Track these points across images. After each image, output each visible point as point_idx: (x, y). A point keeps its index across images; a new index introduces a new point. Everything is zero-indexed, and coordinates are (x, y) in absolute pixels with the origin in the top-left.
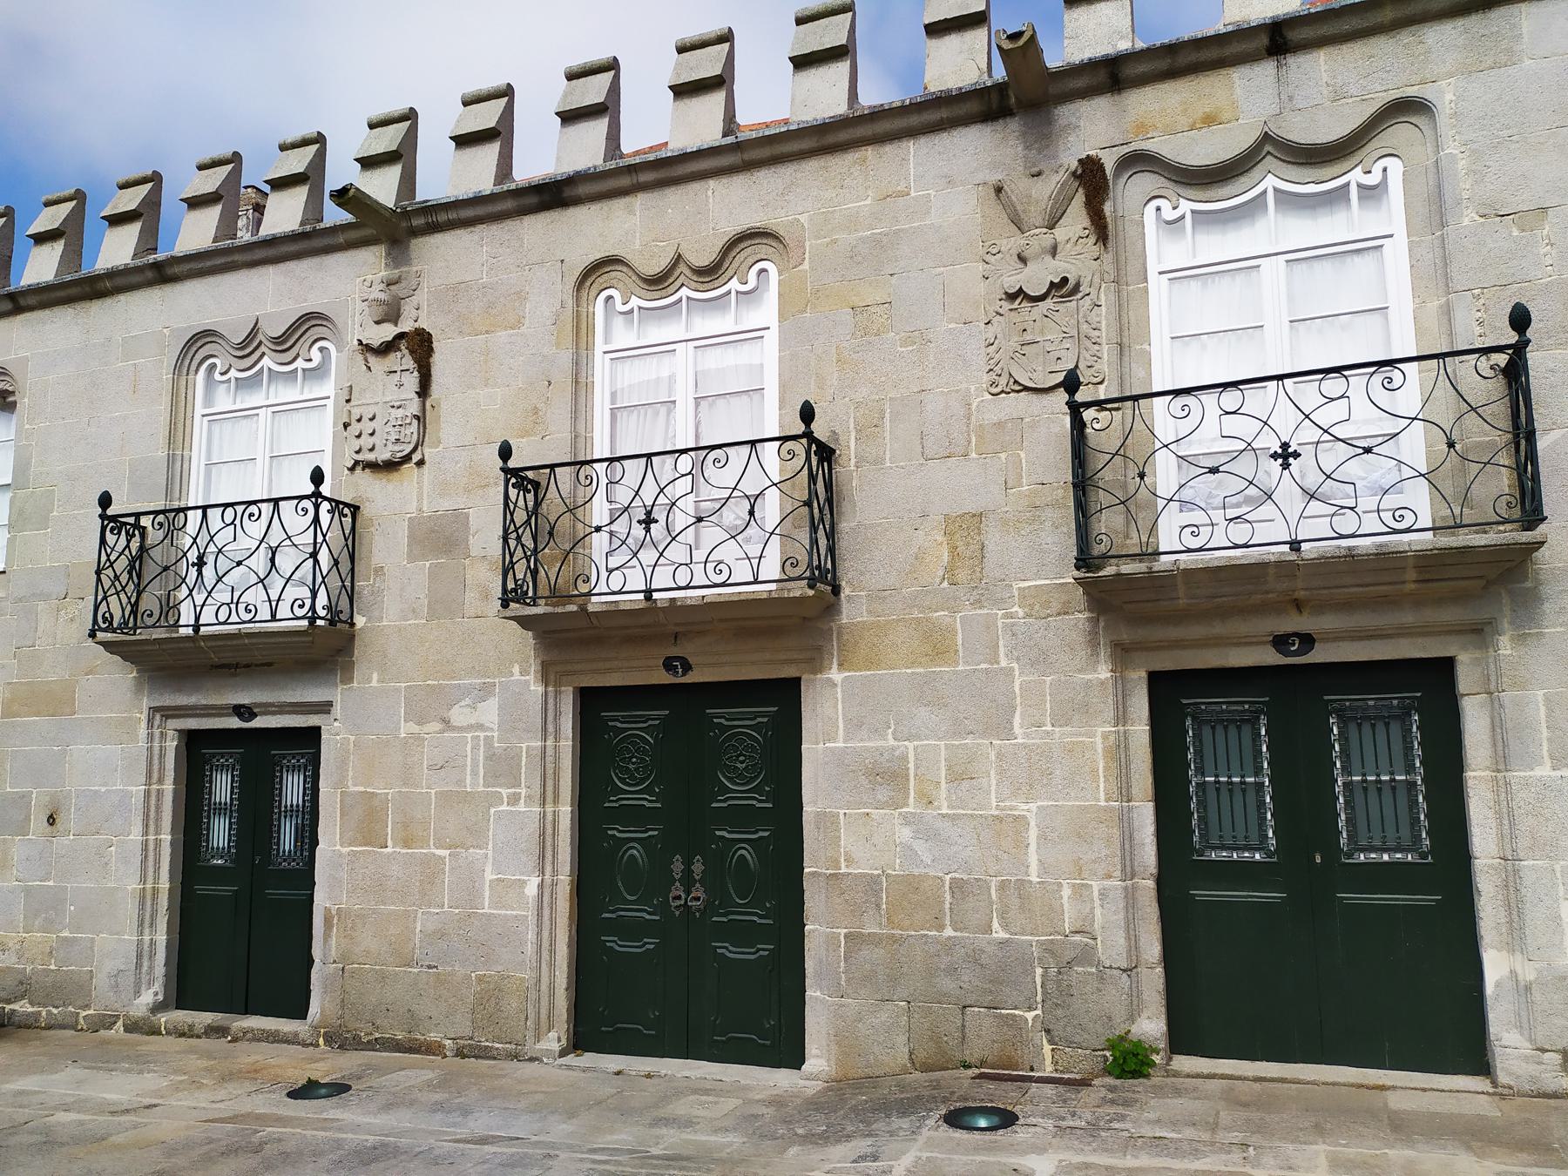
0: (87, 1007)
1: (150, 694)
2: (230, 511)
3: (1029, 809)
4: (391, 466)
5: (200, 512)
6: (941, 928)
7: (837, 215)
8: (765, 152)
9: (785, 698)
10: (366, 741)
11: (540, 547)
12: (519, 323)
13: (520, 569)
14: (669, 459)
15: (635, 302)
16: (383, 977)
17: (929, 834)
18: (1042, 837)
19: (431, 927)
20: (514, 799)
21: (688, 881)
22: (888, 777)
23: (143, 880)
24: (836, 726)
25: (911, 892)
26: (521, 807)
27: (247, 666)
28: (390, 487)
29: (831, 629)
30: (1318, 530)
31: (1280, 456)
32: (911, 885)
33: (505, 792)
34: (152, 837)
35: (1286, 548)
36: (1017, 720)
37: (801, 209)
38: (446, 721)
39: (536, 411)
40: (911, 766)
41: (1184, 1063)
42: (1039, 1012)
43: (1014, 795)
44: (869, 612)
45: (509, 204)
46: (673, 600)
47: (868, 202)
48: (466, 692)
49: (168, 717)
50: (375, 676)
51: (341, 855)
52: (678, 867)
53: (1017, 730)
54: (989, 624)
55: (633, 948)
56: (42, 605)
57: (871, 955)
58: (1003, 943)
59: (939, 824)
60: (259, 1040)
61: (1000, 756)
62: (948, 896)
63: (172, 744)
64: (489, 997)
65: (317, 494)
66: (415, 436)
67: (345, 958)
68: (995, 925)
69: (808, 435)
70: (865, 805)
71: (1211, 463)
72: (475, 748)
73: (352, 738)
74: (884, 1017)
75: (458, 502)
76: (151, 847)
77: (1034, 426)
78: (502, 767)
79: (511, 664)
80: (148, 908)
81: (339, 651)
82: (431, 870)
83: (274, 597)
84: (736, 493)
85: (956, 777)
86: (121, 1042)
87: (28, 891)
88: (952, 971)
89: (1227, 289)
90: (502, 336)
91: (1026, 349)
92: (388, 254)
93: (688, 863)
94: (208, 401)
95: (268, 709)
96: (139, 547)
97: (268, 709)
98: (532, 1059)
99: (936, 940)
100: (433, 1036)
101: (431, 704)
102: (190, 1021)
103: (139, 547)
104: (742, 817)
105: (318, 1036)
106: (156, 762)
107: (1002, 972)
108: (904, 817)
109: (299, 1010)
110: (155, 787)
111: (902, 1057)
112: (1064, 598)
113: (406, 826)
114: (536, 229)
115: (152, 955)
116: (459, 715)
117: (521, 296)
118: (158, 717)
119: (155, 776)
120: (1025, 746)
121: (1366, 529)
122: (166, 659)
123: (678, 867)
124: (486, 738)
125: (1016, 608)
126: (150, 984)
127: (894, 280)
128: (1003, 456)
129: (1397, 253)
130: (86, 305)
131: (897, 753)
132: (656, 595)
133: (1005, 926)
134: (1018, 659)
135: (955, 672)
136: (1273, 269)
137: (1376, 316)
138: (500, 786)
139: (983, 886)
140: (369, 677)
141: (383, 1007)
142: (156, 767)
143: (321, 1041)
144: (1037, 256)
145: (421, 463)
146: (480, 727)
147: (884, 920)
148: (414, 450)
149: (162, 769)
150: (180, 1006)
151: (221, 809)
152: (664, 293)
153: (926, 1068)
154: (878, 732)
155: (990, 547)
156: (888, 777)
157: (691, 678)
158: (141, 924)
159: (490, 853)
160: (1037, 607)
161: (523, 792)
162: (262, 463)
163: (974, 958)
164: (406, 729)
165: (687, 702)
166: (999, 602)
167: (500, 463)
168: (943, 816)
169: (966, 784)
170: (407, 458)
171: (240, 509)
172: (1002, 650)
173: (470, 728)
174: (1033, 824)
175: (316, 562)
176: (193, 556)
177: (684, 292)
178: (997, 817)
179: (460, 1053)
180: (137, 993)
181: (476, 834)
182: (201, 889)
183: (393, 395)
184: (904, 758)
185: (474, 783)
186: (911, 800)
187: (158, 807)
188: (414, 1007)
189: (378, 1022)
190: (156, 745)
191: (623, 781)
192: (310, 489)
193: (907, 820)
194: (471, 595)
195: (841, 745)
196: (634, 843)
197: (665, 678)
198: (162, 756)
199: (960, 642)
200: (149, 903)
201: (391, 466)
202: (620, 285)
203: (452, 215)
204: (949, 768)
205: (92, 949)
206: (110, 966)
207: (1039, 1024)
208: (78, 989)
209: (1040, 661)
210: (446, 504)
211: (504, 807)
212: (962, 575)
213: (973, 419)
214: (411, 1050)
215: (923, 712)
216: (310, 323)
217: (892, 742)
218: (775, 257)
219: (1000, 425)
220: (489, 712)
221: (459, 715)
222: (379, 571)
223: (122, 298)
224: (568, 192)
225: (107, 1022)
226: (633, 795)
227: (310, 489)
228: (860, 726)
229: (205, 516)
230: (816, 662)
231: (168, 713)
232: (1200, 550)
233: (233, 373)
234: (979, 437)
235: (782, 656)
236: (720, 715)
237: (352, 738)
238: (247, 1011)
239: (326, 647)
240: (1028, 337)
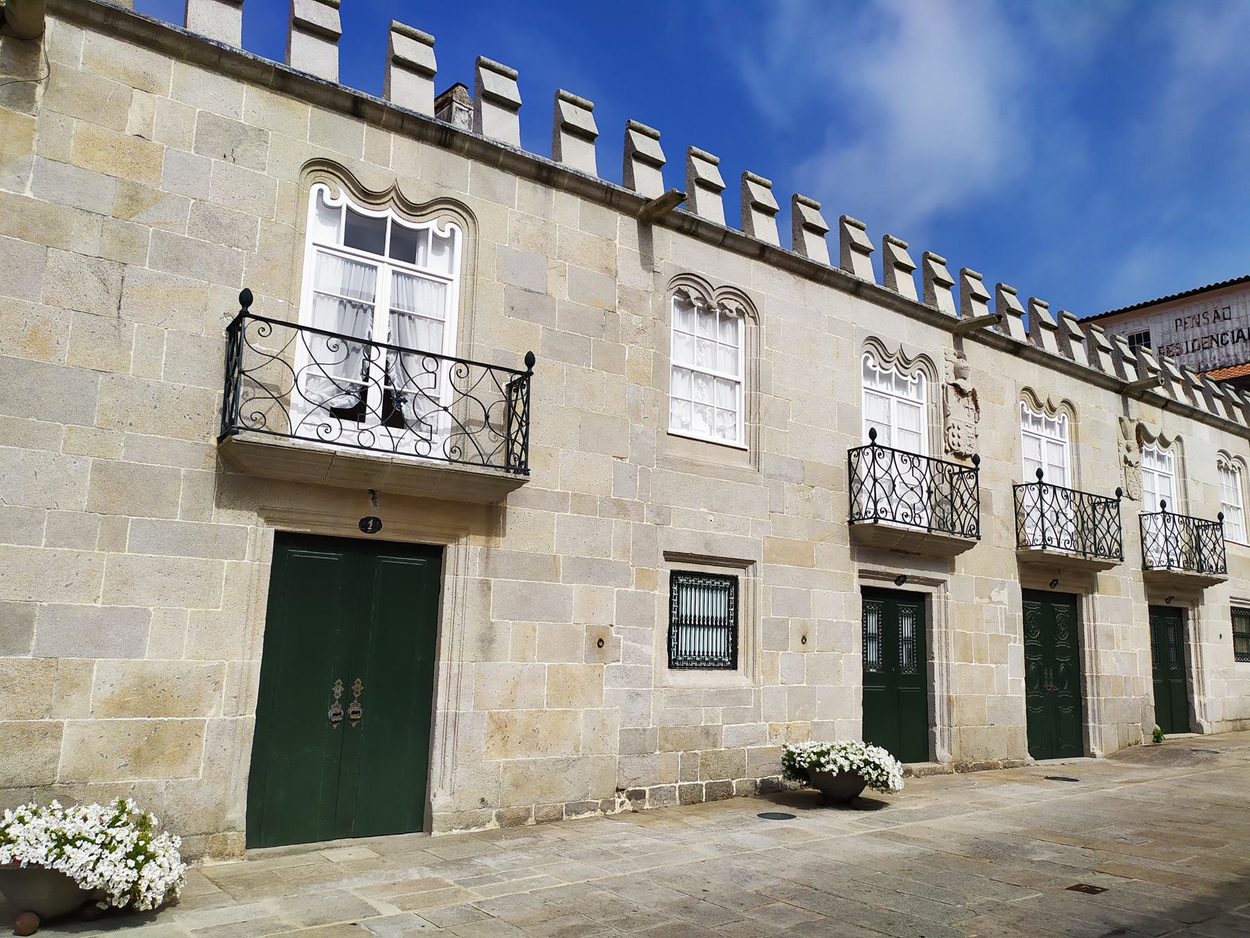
9: (1073, 601)
41: (1166, 736)
45: (599, 194)
56: (786, 485)
65: (873, 444)
87: (791, 690)
100: (995, 760)
116: (995, 596)
146: (1001, 603)
164: (977, 600)
185: (1002, 632)
192: (869, 442)
214: (989, 768)
227: (1037, 480)
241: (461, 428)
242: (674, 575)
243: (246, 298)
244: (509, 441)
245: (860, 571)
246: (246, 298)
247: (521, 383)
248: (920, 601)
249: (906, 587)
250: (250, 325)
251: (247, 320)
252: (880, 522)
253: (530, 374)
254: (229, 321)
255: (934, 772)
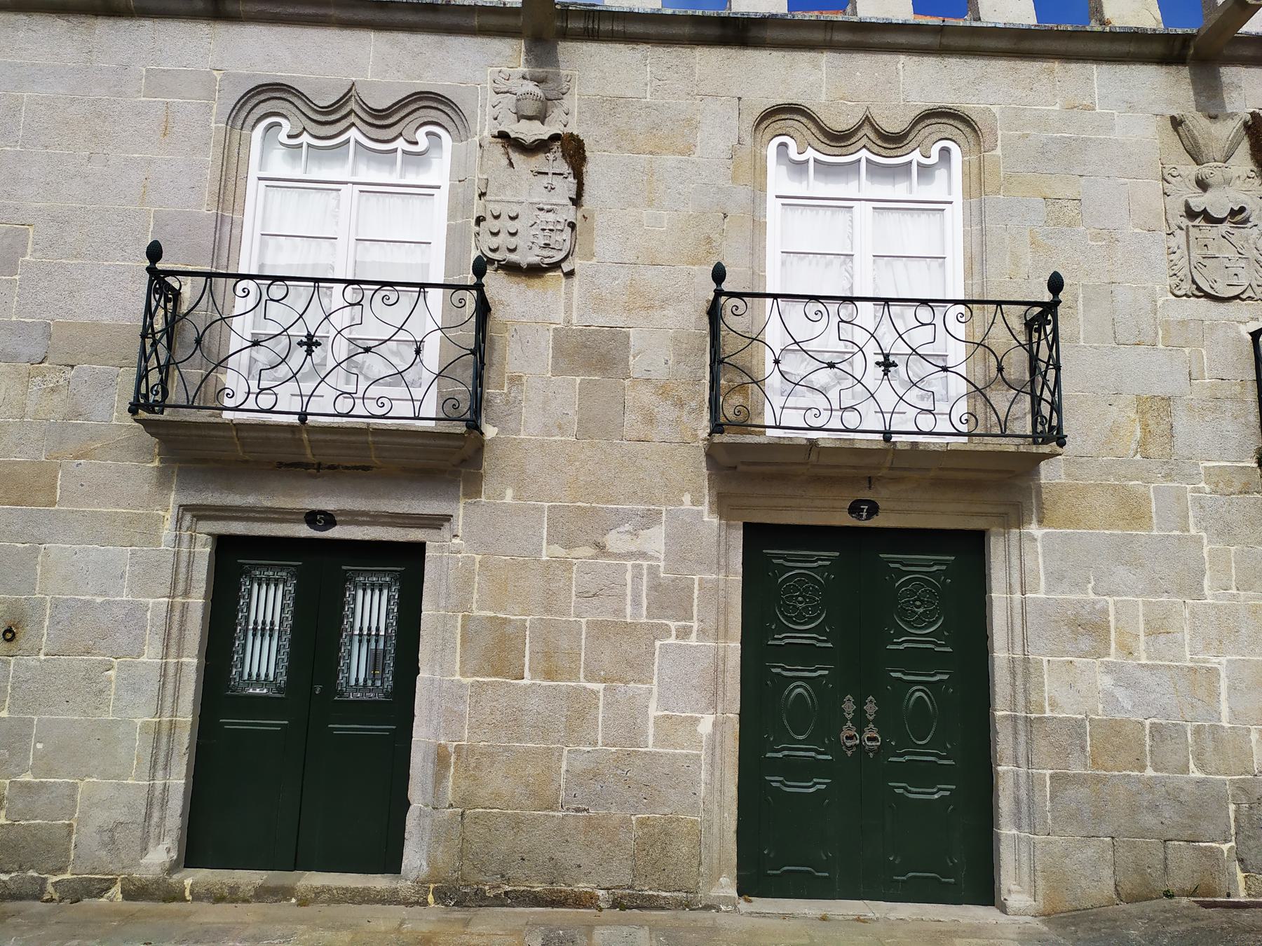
0: (62, 870)
1: (181, 489)
3: (1220, 662)
4: (535, 271)
6: (1142, 768)
7: (1027, 113)
8: (964, 42)
9: (970, 550)
11: (179, 355)
12: (688, 150)
13: (154, 377)
15: (811, 154)
16: (517, 824)
17: (1130, 684)
18: (1232, 688)
19: (579, 766)
20: (684, 633)
21: (860, 721)
22: (1090, 629)
23: (159, 711)
24: (1028, 578)
25: (1114, 738)
26: (693, 641)
27: (332, 467)
28: (530, 293)
29: (1029, 487)
30: (326, 405)
31: (305, 344)
32: (1113, 728)
33: (673, 625)
34: (172, 660)
35: (879, 437)
36: (1206, 583)
37: (992, 100)
38: (600, 547)
39: (709, 240)
40: (1112, 618)
42: (1233, 844)
43: (1207, 647)
44: (1068, 475)
46: (915, 444)
47: (1057, 107)
48: (626, 517)
49: (199, 518)
50: (509, 493)
51: (462, 686)
52: (849, 706)
53: (1206, 591)
54: (1180, 497)
55: (795, 787)
57: (1073, 793)
58: (1199, 783)
59: (1138, 673)
60: (338, 902)
61: (1193, 614)
62: (1147, 739)
63: (204, 551)
64: (655, 842)
66: (568, 243)
67: (466, 801)
68: (1192, 766)
69: (479, 287)
70: (1067, 653)
71: (827, 358)
72: (637, 577)
73: (478, 558)
74: (1090, 852)
75: (618, 320)
76: (171, 671)
77: (1212, 328)
78: (671, 599)
79: (682, 491)
80: (163, 746)
81: (464, 462)
82: (581, 707)
83: (1003, 419)
84: (402, 336)
85: (1154, 631)
86: (118, 913)
88: (1154, 808)
89: (317, 199)
90: (670, 160)
91: (1206, 262)
92: (528, 51)
93: (860, 703)
94: (262, 166)
95: (354, 518)
96: (174, 315)
97: (354, 518)
98: (707, 908)
99: (1139, 780)
100: (582, 886)
101: (583, 526)
102: (231, 882)
103: (174, 315)
104: (920, 660)
105: (427, 892)
106: (183, 570)
107: (1198, 809)
108: (1107, 665)
109: (390, 862)
110: (179, 599)
111: (1109, 890)
112: (1244, 479)
113: (548, 656)
114: (710, 62)
115: (164, 803)
116: (616, 541)
117: (692, 124)
118: (188, 517)
119: (181, 587)
120: (1215, 606)
122: (196, 447)
123: (849, 706)
124: (650, 567)
125: (1202, 485)
126: (159, 839)
127: (1082, 180)
128: (1187, 350)
129: (955, 215)
130: (90, 21)
131: (1097, 607)
132: (895, 438)
133: (1201, 767)
134: (1206, 529)
135: (1150, 537)
136: (863, 211)
137: (935, 263)
138: (668, 618)
139: (1181, 731)
140: (500, 493)
141: (518, 856)
142: (182, 576)
143: (430, 898)
144: (1219, 185)
145: (570, 274)
146: (643, 555)
147: (1089, 762)
148: (566, 257)
149: (189, 579)
150: (188, 865)
151: (263, 631)
152: (844, 150)
153: (1133, 899)
154: (1079, 586)
155: (1178, 428)
156: (1090, 629)
157: (877, 522)
158: (154, 766)
159: (655, 689)
160: (1221, 485)
161: (695, 625)
163: (1174, 796)
165: (861, 546)
166: (1188, 477)
168: (1143, 666)
169: (1162, 638)
170: (556, 266)
172: (1191, 520)
173: (631, 555)
174: (1223, 675)
177: (353, 134)
178: (1191, 669)
179: (617, 904)
180: (144, 850)
181: (638, 667)
182: (231, 723)
183: (542, 198)
184: (1105, 611)
186: (1113, 650)
187: (182, 624)
188: (558, 855)
189: (510, 873)
190: (184, 549)
191: (789, 619)
193: (1109, 669)
194: (629, 418)
195: (1042, 596)
196: (799, 681)
197: (847, 520)
198: (190, 564)
199: (1154, 510)
200: (164, 740)
201: (535, 271)
202: (797, 135)
203: (618, 27)
204: (1147, 622)
205: (72, 797)
206: (102, 817)
207: (1234, 856)
208: (51, 849)
209: (1225, 532)
210: (599, 320)
211: (672, 640)
212: (1153, 450)
213: (1158, 314)
214: (553, 903)
215: (1121, 571)
216: (427, 103)
217: (1092, 596)
218: (961, 139)
219: (1183, 323)
220: (655, 540)
221: (616, 541)
222: (516, 380)
223: (148, 24)
224: (754, 32)
225: (101, 888)
226: (802, 635)
227: (471, 279)
228: (1061, 579)
230: (1015, 516)
231: (200, 513)
232: (383, 417)
233: (305, 138)
234: (1166, 331)
235: (975, 509)
236: (892, 558)
237: (478, 558)
239: (450, 457)
240: (1210, 253)
241: (978, 392)
242: (225, 547)
243: (719, 274)
244: (1036, 401)
245: (185, 508)
246: (719, 274)
247: (1042, 317)
248: (404, 564)
249: (335, 533)
250: (728, 303)
251: (723, 299)
252: (895, 438)
253: (1055, 303)
254: (705, 306)
255: (392, 899)
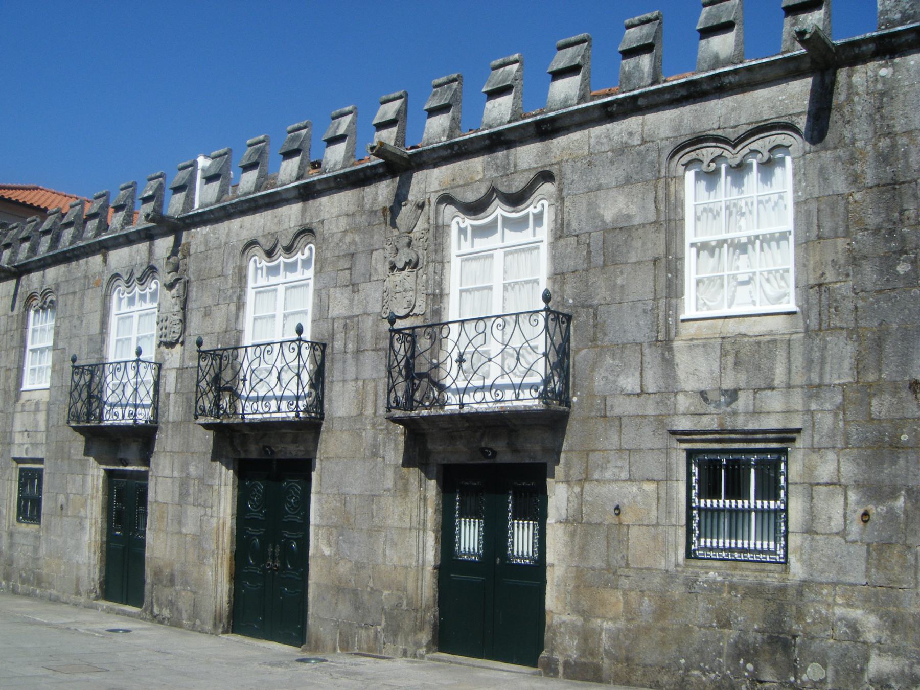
2: (481, 323)
5: (514, 317)
10: (163, 480)
14: (473, 324)
93: (274, 548)
121: (510, 401)
162: (498, 291)
167: (196, 348)
171: (262, 347)
175: (299, 378)
176: (455, 356)
177: (281, 258)
192: (296, 336)
227: (296, 336)
229: (517, 321)
238: (127, 603)
